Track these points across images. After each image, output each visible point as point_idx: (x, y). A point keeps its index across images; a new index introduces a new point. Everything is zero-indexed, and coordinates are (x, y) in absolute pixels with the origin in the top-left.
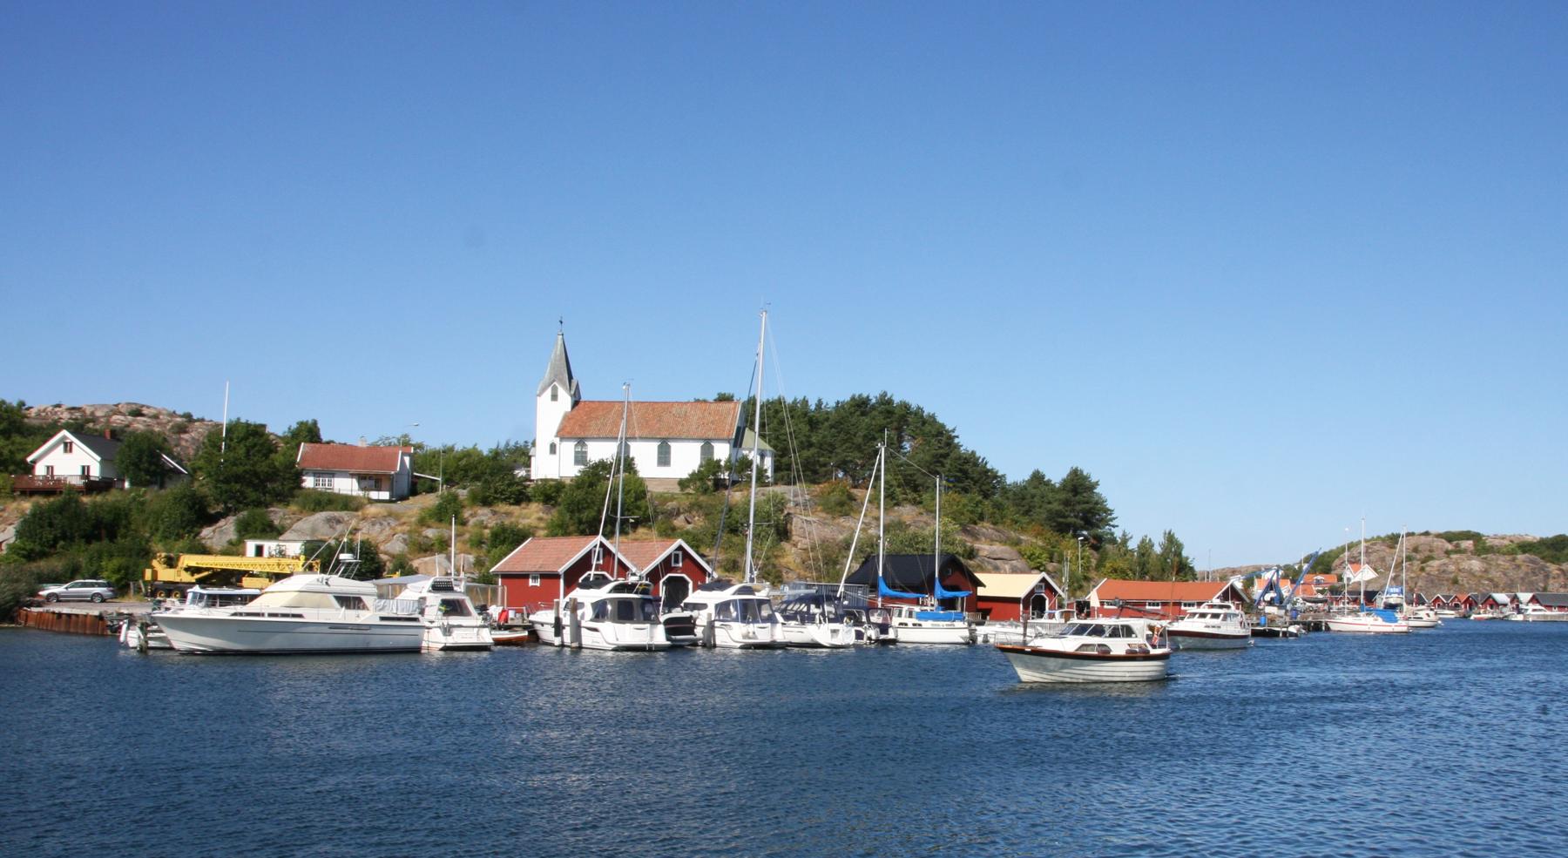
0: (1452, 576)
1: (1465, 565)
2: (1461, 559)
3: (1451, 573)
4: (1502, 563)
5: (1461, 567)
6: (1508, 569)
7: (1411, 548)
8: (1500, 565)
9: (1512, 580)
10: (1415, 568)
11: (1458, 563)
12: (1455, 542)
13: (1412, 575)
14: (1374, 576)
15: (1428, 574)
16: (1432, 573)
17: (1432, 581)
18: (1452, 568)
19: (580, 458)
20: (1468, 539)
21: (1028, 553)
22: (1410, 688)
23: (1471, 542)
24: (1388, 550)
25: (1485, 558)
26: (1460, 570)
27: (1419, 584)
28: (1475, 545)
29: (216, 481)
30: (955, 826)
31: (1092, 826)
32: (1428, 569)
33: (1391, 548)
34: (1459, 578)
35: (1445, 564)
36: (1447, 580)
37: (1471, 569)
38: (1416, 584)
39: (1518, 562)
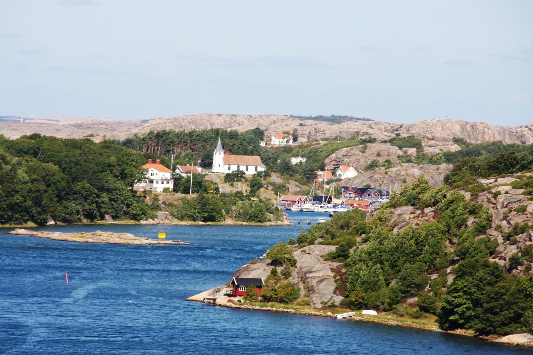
0: (403, 178)
1: (411, 171)
2: (408, 167)
3: (403, 176)
4: (431, 171)
5: (408, 173)
6: (434, 175)
7: (376, 153)
8: (430, 172)
9: (436, 182)
10: (382, 172)
11: (407, 170)
12: (404, 149)
13: (381, 176)
14: (356, 175)
15: (389, 176)
16: (392, 176)
17: (392, 181)
18: (403, 173)
19: (256, 170)
20: (413, 147)
21: (489, 246)
22: (249, 252)
23: (415, 149)
24: (361, 154)
25: (421, 168)
26: (407, 175)
27: (385, 182)
28: (417, 152)
29: (162, 179)
30: (70, 348)
31: (255, 337)
32: (389, 173)
33: (363, 153)
34: (407, 180)
35: (399, 170)
36: (400, 180)
37: (414, 174)
38: (383, 182)
39: (440, 170)
